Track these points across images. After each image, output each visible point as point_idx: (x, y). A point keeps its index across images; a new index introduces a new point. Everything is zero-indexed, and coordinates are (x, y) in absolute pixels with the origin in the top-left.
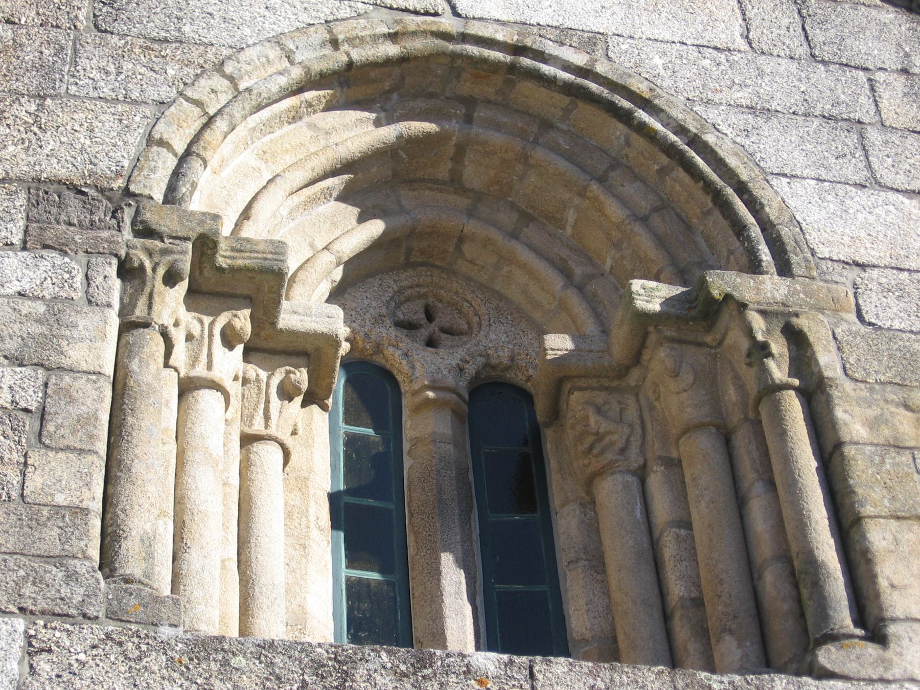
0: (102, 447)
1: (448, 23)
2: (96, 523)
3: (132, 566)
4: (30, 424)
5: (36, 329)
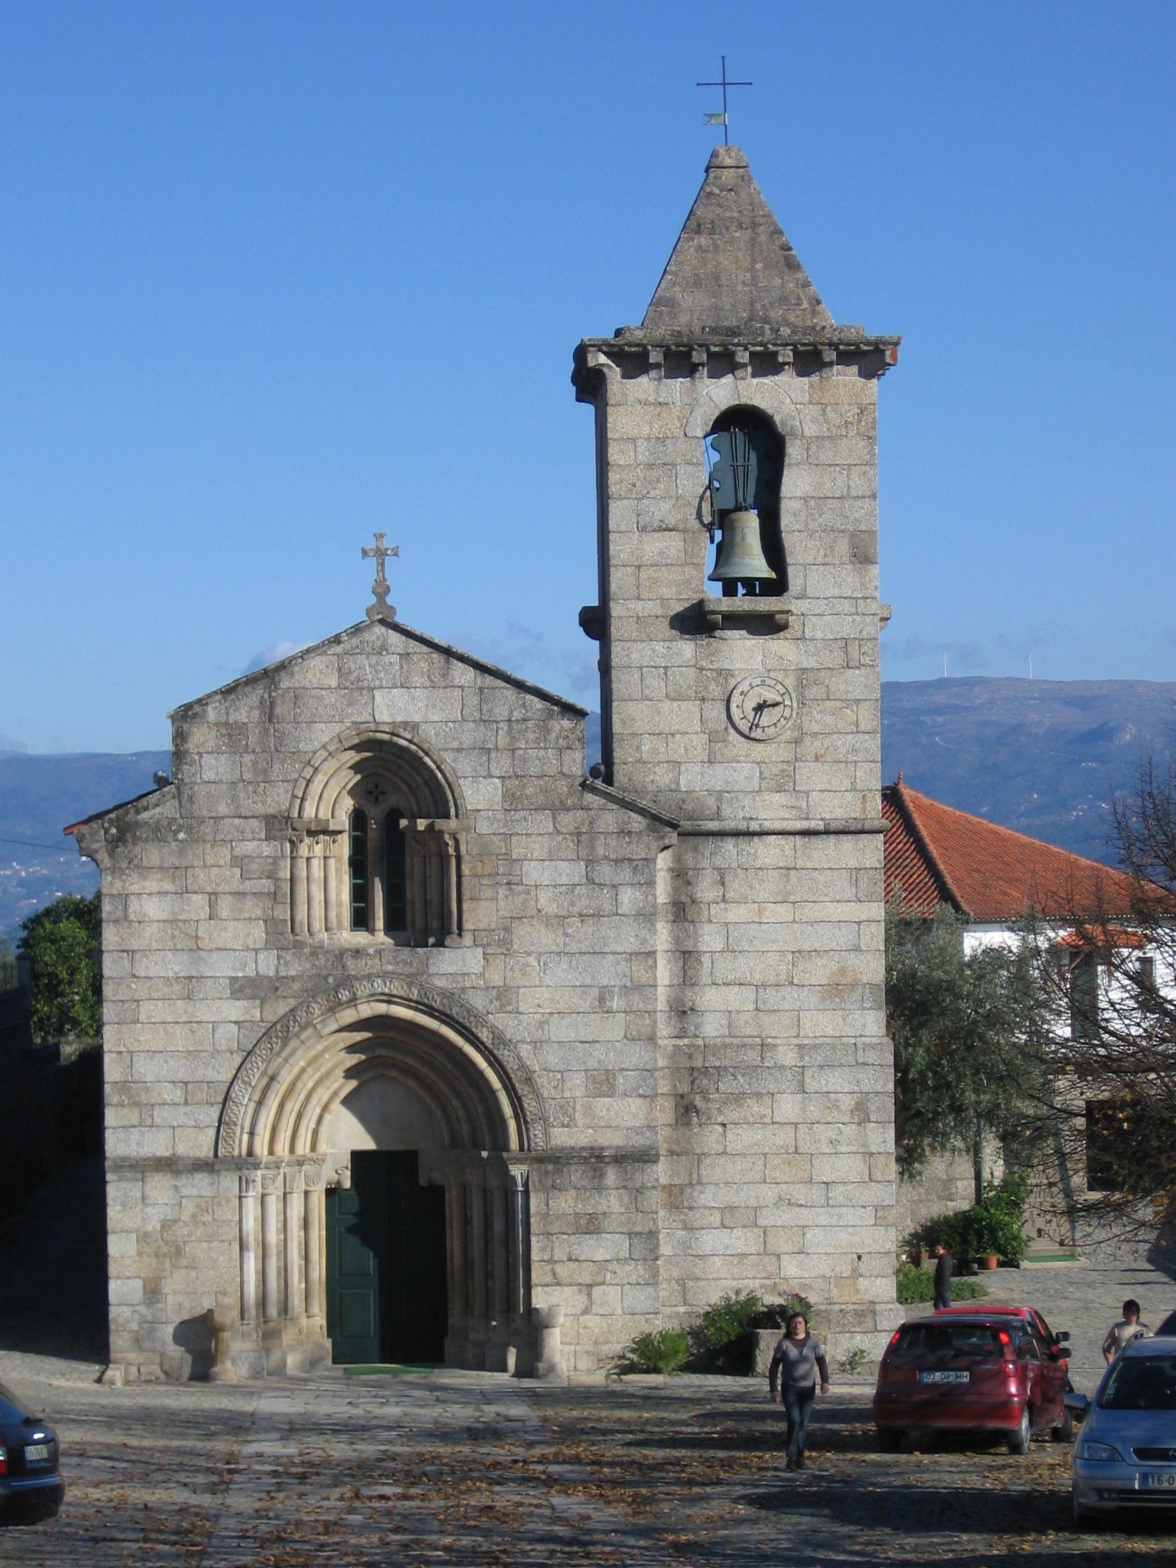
0: (289, 901)
1: (372, 726)
2: (289, 922)
3: (298, 931)
4: (272, 896)
5: (272, 867)
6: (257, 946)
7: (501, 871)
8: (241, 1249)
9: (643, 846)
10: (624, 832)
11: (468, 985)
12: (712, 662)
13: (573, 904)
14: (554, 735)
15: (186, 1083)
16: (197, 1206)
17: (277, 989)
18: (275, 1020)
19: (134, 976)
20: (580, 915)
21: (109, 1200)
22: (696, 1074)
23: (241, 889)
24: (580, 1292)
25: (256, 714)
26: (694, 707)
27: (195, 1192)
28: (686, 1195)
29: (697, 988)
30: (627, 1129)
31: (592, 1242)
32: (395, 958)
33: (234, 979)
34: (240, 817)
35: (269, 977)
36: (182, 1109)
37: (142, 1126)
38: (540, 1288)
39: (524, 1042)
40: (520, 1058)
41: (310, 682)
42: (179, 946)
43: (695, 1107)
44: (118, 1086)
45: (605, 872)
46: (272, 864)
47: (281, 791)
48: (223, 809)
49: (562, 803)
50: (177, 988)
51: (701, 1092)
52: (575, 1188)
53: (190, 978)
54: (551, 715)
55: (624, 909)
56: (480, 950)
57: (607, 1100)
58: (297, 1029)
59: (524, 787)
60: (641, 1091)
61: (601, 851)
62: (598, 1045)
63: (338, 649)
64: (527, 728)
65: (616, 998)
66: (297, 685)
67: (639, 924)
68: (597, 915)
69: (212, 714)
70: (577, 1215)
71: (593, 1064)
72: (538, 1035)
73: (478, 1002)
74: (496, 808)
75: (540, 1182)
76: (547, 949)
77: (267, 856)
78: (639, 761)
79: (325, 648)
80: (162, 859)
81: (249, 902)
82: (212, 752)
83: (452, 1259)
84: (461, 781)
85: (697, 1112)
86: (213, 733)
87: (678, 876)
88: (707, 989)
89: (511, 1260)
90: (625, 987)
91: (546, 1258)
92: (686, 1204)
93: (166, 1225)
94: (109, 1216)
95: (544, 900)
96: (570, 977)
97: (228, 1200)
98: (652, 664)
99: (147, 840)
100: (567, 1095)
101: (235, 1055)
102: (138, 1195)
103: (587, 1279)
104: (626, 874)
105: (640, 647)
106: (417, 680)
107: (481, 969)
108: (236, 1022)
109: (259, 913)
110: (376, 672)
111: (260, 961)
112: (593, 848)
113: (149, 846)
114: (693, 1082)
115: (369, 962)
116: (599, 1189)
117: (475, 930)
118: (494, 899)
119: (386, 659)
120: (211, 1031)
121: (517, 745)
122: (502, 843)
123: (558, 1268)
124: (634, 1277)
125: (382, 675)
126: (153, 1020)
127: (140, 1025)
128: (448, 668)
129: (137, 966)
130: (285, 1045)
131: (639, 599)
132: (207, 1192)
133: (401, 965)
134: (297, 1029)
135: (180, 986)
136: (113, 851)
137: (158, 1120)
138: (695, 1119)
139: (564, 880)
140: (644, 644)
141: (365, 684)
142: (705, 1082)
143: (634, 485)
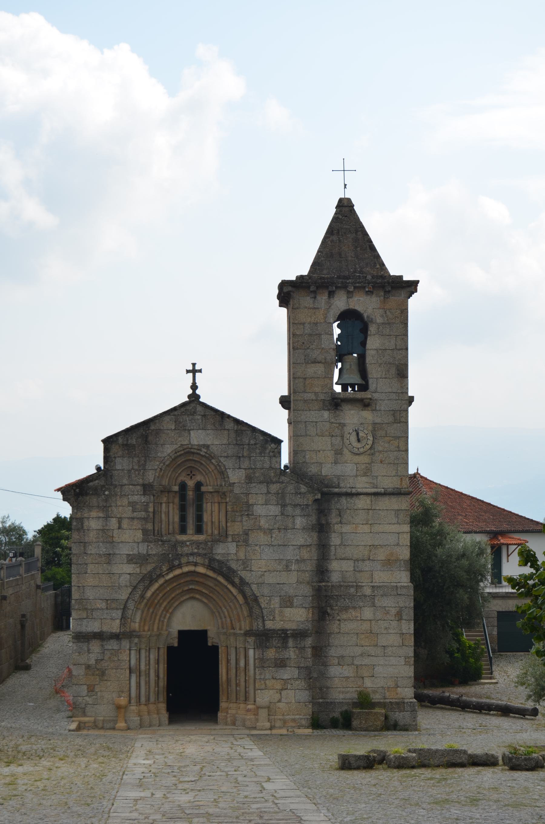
6: (139, 541)
8: (130, 673)
12: (336, 420)
13: (275, 524)
15: (107, 600)
17: (147, 559)
19: (85, 553)
23: (132, 516)
26: (328, 439)
29: (329, 561)
30: (298, 622)
33: (129, 555)
34: (132, 485)
37: (88, 618)
38: (259, 691)
43: (327, 612)
44: (78, 601)
46: (145, 505)
48: (125, 481)
49: (271, 480)
52: (275, 647)
55: (297, 526)
56: (235, 543)
59: (254, 473)
60: (304, 605)
64: (256, 447)
65: (293, 565)
66: (157, 428)
67: (304, 533)
69: (120, 440)
71: (283, 593)
72: (260, 580)
73: (234, 566)
82: (121, 457)
83: (222, 677)
84: (228, 470)
85: (328, 615)
89: (247, 678)
92: (323, 655)
95: (263, 522)
96: (274, 555)
97: (125, 651)
98: (311, 420)
100: (272, 606)
101: (129, 588)
102: (86, 649)
107: (235, 552)
108: (129, 574)
109: (140, 526)
110: (192, 422)
111: (140, 547)
117: (233, 535)
118: (241, 521)
120: (118, 577)
121: (252, 455)
122: (245, 497)
123: (267, 682)
124: (300, 687)
126: (94, 573)
127: (88, 575)
132: (116, 647)
133: (201, 550)
137: (95, 616)
138: (327, 618)
140: (307, 412)
141: (187, 428)
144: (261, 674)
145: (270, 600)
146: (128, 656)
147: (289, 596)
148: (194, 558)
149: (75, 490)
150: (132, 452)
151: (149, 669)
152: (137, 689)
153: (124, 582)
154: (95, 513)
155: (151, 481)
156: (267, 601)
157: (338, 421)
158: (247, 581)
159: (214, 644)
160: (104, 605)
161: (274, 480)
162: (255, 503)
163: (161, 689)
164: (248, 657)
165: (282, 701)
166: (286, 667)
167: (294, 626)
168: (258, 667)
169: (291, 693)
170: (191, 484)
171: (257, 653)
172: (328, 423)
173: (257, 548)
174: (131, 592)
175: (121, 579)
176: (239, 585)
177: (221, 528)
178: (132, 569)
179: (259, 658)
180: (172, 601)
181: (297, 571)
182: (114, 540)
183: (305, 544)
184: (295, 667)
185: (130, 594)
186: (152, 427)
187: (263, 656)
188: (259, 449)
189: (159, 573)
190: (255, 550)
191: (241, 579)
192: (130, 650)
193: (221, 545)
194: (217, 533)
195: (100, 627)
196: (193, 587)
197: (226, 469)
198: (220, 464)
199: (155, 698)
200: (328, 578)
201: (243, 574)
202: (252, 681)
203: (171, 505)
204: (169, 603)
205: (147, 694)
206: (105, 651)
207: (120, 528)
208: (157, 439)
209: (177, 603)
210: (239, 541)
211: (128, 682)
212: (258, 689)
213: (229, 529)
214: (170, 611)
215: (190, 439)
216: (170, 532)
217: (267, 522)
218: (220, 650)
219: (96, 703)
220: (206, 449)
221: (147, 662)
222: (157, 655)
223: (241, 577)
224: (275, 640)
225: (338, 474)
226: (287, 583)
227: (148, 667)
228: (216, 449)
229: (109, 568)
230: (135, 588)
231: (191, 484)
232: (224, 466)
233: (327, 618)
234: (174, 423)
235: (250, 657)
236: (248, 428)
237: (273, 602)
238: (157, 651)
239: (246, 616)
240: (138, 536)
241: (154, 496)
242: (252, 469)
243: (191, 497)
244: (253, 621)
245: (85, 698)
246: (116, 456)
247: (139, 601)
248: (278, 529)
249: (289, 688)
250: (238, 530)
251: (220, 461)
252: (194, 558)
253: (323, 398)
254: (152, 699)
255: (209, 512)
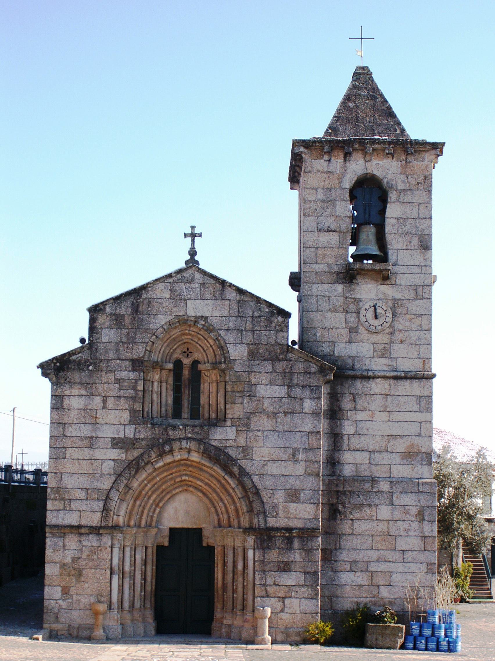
6: (125, 423)
7: (246, 389)
9: (316, 379)
10: (307, 373)
11: (228, 445)
12: (351, 294)
13: (280, 407)
14: (274, 325)
15: (87, 489)
16: (91, 551)
17: (134, 444)
18: (132, 459)
19: (65, 436)
20: (284, 413)
21: (47, 547)
22: (339, 494)
24: (279, 601)
25: (130, 310)
26: (342, 316)
27: (90, 544)
28: (333, 554)
29: (341, 452)
30: (305, 519)
31: (286, 576)
32: (193, 430)
33: (114, 439)
34: (119, 359)
35: (131, 438)
36: (85, 502)
38: (259, 599)
39: (255, 474)
40: (253, 482)
41: (156, 295)
42: (87, 422)
43: (339, 510)
44: (54, 489)
45: (297, 392)
47: (140, 347)
48: (111, 355)
49: (277, 357)
50: (85, 442)
51: (342, 503)
52: (279, 548)
53: (92, 438)
54: (272, 314)
55: (306, 410)
56: (234, 428)
57: (295, 504)
58: (143, 464)
59: (258, 349)
60: (312, 501)
61: (295, 381)
62: (291, 477)
63: (171, 280)
67: (313, 418)
68: (293, 413)
69: (108, 310)
70: (278, 562)
71: (288, 486)
72: (262, 471)
73: (232, 453)
74: (245, 359)
75: (261, 544)
76: (267, 429)
77: (132, 379)
78: (315, 341)
79: (164, 279)
80: (81, 378)
81: (122, 401)
82: (108, 328)
83: (217, 583)
84: (228, 345)
85: (340, 513)
86: (108, 319)
87: (332, 397)
88: (346, 452)
90: (305, 448)
91: (263, 583)
93: (75, 560)
94: (46, 554)
96: (278, 443)
97: (106, 549)
98: (323, 294)
99: (74, 369)
100: (275, 501)
101: (112, 476)
102: (61, 544)
103: (282, 594)
104: (307, 393)
105: (317, 286)
106: (208, 296)
107: (235, 438)
108: (113, 460)
109: (127, 406)
110: (189, 291)
111: (126, 430)
112: (291, 380)
113: (75, 372)
114: (338, 498)
115: (180, 432)
116: (291, 549)
117: (232, 418)
118: (242, 403)
119: (194, 285)
120: (100, 464)
121: (256, 328)
122: (247, 376)
123: (269, 588)
124: (306, 595)
125: (191, 293)
128: (224, 291)
129: (67, 430)
130: (137, 472)
131: (317, 263)
133: (196, 434)
134: (143, 464)
135: (87, 441)
136: (58, 374)
137: (73, 507)
138: (339, 516)
139: (277, 395)
140: (319, 285)
141: (183, 297)
142: (344, 498)
143: (316, 210)
144: (261, 579)
145: (273, 494)
146: (110, 554)
147: (296, 490)
148: (187, 443)
149: (55, 364)
150: (121, 322)
151: (134, 570)
152: (119, 593)
153: (107, 469)
154: (77, 391)
155: (141, 355)
156: (270, 495)
157: (353, 296)
158: (247, 471)
159: (210, 544)
160: (83, 495)
161: (281, 357)
162: (259, 382)
163: (148, 594)
164: (247, 559)
165: (286, 611)
166: (290, 571)
167: (299, 524)
168: (258, 571)
169: (296, 602)
170: (187, 361)
171: (257, 554)
172: (342, 298)
173: (260, 434)
174: (115, 481)
175: (103, 466)
176: (238, 476)
177: (219, 411)
178: (117, 454)
179: (259, 561)
180: (163, 494)
181: (305, 461)
182: (98, 421)
183: (315, 430)
184: (301, 572)
185: (114, 483)
186: (144, 296)
187: (264, 559)
188: (264, 322)
189: (147, 460)
190: (258, 436)
191: (240, 467)
192: (112, 548)
193: (219, 430)
194: (215, 417)
195: (79, 520)
196: (187, 478)
197: (226, 343)
198: (219, 338)
199: (141, 604)
200: (340, 472)
201: (243, 463)
202: (250, 586)
203: (164, 384)
204: (159, 495)
205: (132, 599)
206: (84, 548)
207: (104, 408)
208: (149, 309)
209: (168, 496)
210: (239, 426)
211: (109, 585)
212: (258, 597)
213: (228, 412)
214: (161, 505)
215: (186, 310)
216: (162, 415)
217: (272, 405)
218: (216, 551)
219: (70, 608)
220: (204, 321)
221: (132, 563)
222: (144, 555)
223: (240, 466)
224: (279, 539)
225: (353, 355)
226: (293, 474)
227: (133, 568)
228: (215, 321)
229: (91, 453)
230: (119, 476)
231: (187, 361)
232: (224, 341)
233: (339, 516)
234: (169, 291)
235: (249, 559)
236: (252, 298)
237: (276, 496)
238: (144, 551)
239: (245, 511)
240: (125, 417)
241: (144, 372)
242: (255, 344)
243: (187, 376)
244: (253, 517)
245: (58, 601)
246: (103, 326)
247: (123, 491)
248: (284, 413)
249: (293, 596)
250: (238, 413)
251: (220, 335)
252: (187, 443)
253: (337, 270)
254: (137, 605)
255: (206, 394)
